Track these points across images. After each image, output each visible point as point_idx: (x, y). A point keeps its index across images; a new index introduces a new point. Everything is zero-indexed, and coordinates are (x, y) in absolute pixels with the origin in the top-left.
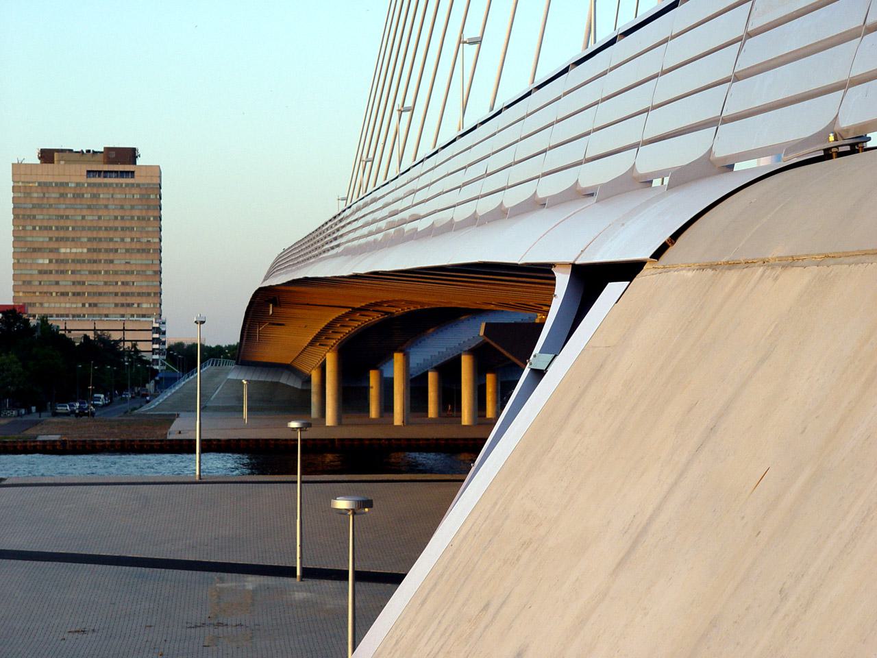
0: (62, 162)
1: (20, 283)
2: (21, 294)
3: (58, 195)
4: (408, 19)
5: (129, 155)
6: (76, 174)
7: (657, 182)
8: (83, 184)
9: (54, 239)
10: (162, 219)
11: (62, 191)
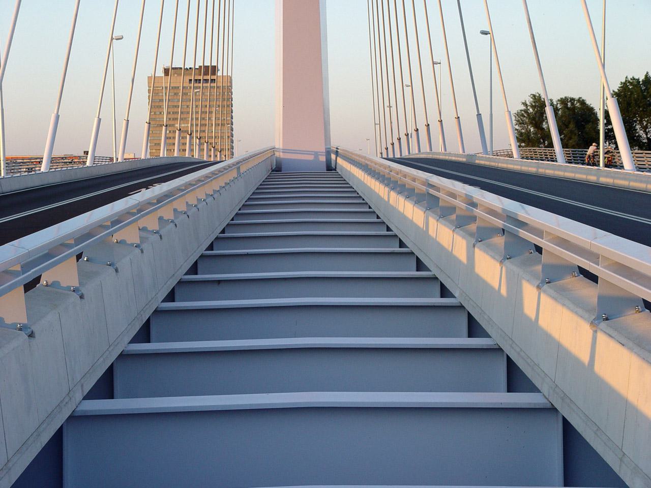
0: (176, 75)
1: (153, 144)
2: (154, 151)
3: (173, 94)
4: (380, 74)
5: (214, 69)
6: (180, 81)
7: (108, 356)
8: (187, 88)
9: (172, 119)
10: (233, 100)
11: (175, 92)
